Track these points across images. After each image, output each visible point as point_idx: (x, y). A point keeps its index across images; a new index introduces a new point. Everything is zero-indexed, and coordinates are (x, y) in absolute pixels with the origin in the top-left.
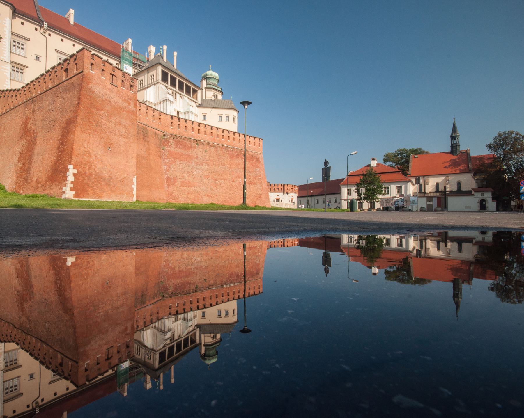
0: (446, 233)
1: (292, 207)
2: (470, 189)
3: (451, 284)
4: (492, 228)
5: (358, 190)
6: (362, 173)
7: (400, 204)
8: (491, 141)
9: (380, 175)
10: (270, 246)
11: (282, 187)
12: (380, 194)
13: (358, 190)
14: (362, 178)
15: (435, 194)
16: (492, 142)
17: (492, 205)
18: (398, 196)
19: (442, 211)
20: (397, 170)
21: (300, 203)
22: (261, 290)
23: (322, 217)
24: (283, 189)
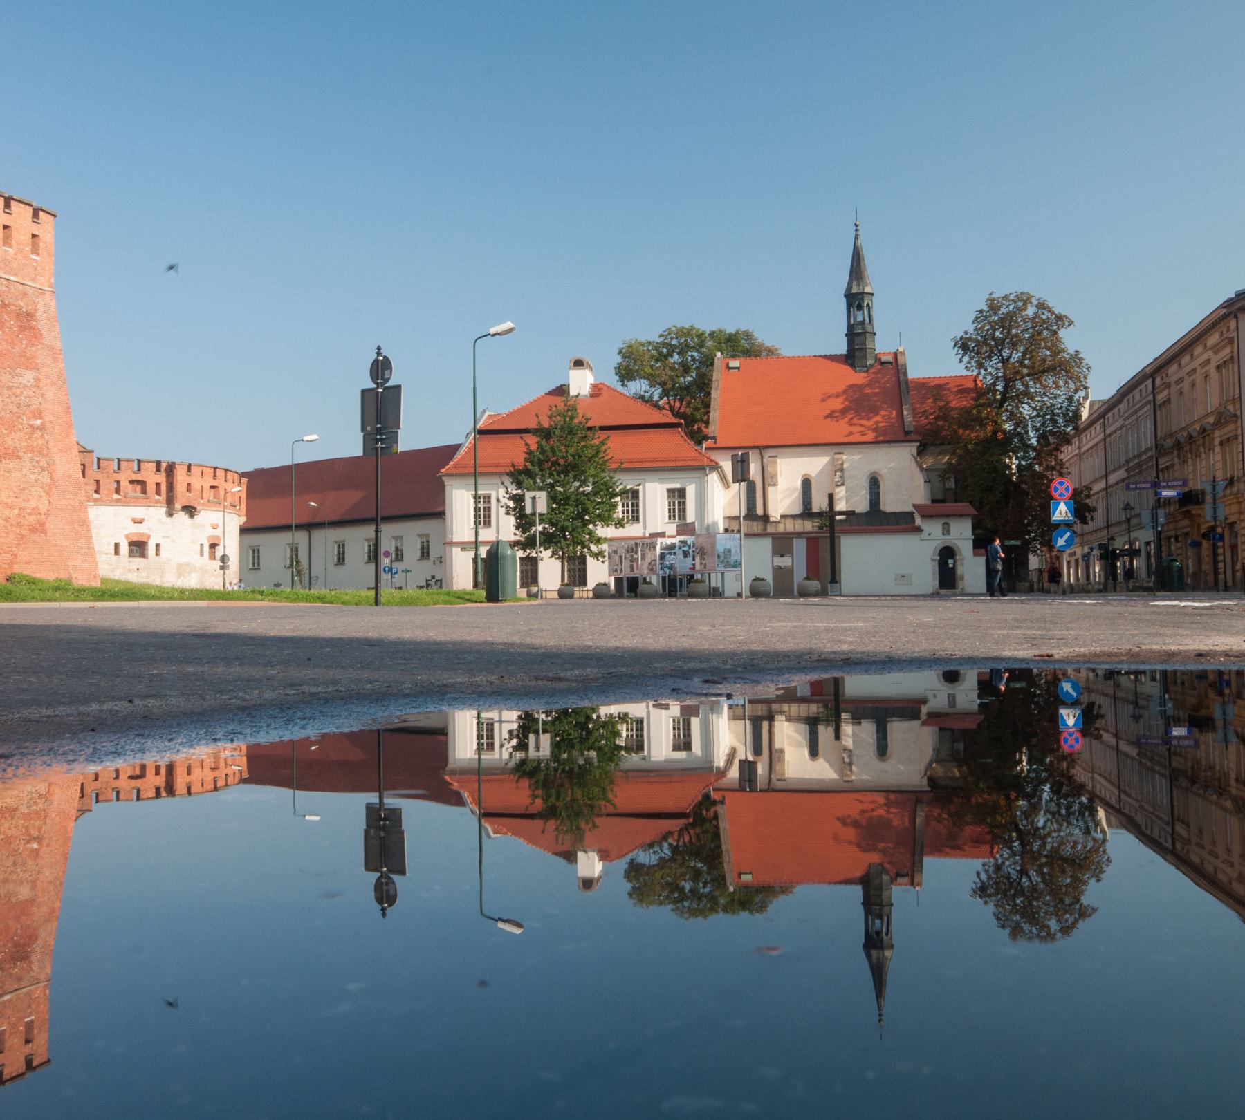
0: (837, 682)
1: (214, 581)
2: (910, 509)
3: (857, 891)
4: (971, 661)
5: (518, 500)
6: (532, 425)
7: (682, 565)
8: (965, 325)
9: (603, 435)
10: (89, 797)
11: (161, 477)
12: (606, 519)
13: (518, 500)
14: (534, 447)
15: (799, 526)
16: (971, 328)
17: (972, 569)
18: (672, 529)
19: (823, 593)
20: (668, 418)
21: (253, 560)
22: (40, 1049)
23: (373, 635)
24: (167, 486)
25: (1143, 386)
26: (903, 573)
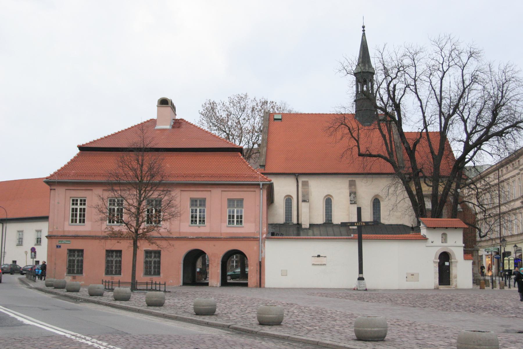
26: (412, 272)
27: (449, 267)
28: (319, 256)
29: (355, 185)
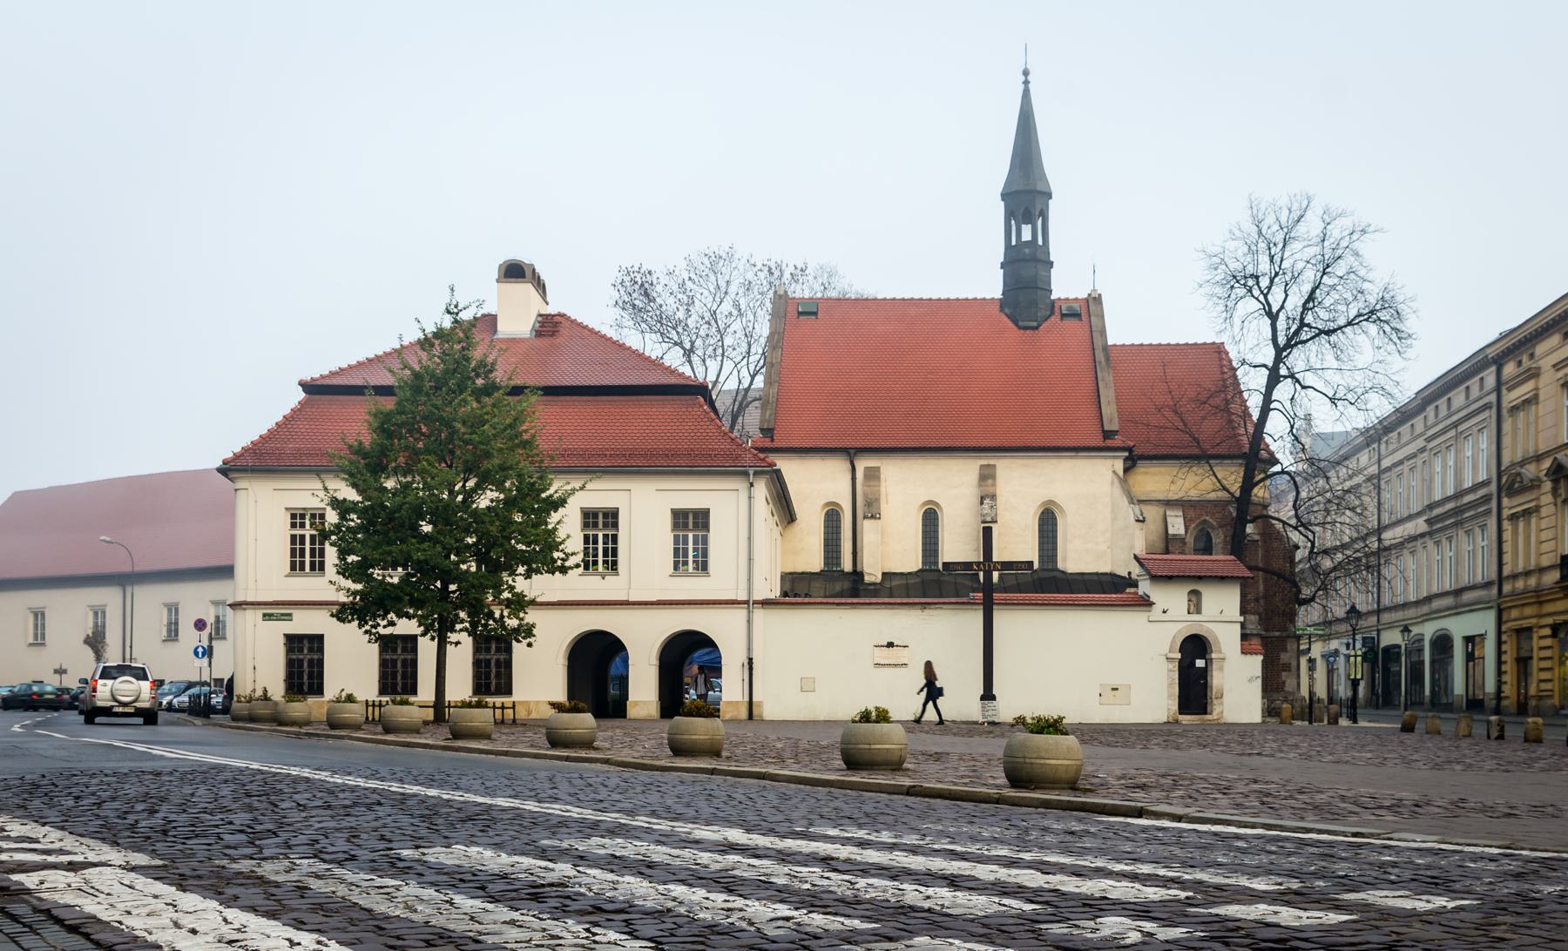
25: (1474, 383)
26: (1114, 683)
27: (1204, 672)
28: (890, 645)
29: (993, 477)
